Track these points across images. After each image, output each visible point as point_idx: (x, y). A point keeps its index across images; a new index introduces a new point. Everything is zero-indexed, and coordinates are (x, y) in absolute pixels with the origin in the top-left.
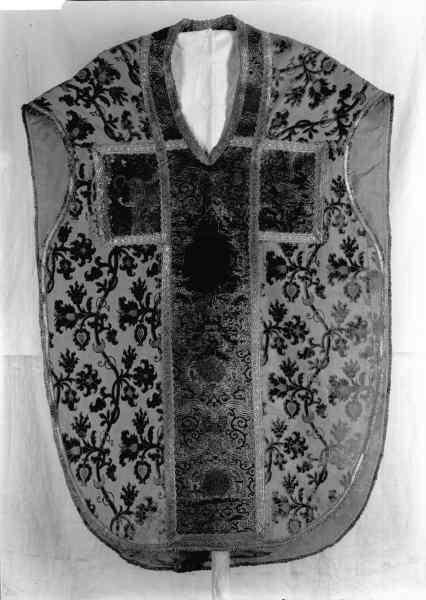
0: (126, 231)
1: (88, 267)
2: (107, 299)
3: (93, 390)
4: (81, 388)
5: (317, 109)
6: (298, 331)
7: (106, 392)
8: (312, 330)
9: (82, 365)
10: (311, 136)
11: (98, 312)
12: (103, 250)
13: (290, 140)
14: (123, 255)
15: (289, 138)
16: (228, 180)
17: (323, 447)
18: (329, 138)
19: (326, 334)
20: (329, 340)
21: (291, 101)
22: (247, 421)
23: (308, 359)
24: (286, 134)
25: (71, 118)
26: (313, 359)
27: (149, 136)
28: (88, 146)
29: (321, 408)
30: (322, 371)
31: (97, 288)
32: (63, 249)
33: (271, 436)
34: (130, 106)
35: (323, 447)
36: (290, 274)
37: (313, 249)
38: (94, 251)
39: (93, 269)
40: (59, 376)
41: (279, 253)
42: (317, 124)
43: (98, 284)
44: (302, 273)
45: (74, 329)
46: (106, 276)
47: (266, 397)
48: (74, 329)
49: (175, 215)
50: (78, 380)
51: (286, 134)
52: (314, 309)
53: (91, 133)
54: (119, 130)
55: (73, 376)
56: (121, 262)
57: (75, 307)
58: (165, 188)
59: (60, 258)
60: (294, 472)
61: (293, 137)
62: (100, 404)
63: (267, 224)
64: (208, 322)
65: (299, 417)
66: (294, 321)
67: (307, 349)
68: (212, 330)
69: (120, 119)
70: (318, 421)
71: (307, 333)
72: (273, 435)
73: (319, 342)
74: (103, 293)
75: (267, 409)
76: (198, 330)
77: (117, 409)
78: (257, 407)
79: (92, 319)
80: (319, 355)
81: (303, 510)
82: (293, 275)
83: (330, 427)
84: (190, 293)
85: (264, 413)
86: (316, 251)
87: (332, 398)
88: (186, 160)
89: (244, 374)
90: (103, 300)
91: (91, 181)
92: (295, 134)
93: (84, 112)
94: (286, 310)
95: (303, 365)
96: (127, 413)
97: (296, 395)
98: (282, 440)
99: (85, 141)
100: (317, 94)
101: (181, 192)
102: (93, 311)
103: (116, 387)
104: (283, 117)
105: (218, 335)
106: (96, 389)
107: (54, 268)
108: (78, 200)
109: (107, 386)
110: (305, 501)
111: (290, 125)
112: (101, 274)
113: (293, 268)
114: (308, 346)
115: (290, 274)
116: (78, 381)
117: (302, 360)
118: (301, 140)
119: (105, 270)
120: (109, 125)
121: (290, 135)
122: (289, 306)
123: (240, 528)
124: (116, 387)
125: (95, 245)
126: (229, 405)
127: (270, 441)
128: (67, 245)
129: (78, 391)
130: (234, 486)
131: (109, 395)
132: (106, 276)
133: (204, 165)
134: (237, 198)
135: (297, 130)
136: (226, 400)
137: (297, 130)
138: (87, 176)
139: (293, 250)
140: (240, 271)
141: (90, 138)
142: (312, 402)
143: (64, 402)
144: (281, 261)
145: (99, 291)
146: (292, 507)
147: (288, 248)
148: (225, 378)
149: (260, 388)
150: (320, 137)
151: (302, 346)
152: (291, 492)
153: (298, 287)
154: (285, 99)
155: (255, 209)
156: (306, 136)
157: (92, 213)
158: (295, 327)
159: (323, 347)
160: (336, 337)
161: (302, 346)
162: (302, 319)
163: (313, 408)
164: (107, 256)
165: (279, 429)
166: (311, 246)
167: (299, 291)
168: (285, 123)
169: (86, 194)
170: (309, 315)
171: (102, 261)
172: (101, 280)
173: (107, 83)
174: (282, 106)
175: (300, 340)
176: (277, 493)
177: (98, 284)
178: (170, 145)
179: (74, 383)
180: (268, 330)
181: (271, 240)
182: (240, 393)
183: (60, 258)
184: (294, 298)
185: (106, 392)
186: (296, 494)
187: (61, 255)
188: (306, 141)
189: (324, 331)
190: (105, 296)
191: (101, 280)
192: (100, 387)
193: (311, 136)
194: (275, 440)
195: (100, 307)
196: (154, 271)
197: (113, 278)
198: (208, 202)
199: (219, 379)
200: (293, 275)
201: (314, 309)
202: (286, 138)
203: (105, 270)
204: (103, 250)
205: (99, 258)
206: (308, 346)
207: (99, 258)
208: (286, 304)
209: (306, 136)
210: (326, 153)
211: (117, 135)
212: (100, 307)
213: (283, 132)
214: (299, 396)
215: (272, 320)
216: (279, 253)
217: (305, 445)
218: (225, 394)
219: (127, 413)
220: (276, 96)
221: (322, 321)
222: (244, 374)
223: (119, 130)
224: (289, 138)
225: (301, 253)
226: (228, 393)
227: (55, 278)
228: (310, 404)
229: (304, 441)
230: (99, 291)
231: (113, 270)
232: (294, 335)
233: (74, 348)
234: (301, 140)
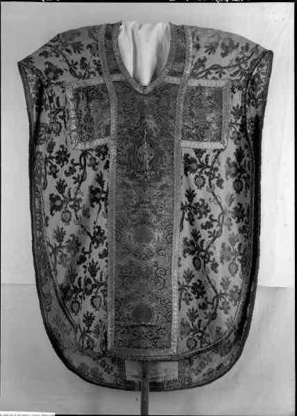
0: (91, 138)
1: (67, 167)
2: (81, 188)
3: (65, 162)
4: (58, 163)
5: (226, 58)
6: (202, 210)
7: (85, 250)
8: (212, 210)
9: (69, 235)
10: (220, 76)
11: (75, 198)
12: (75, 155)
13: (207, 78)
14: (89, 156)
15: (205, 76)
16: (158, 102)
17: (214, 294)
18: (233, 78)
19: (222, 214)
20: (218, 302)
21: (209, 51)
22: (167, 271)
23: (208, 230)
24: (204, 74)
25: (47, 66)
26: (212, 230)
27: (101, 73)
28: (59, 83)
29: (215, 266)
30: (217, 239)
31: (74, 181)
32: (51, 158)
33: (183, 281)
34: (87, 53)
35: (214, 294)
36: (199, 170)
37: (216, 153)
38: (69, 156)
39: (70, 168)
40: (54, 246)
41: (193, 155)
42: (225, 68)
43: (74, 178)
44: (208, 170)
45: (61, 211)
46: (79, 172)
47: (181, 254)
48: (43, 72)
49: (120, 126)
50: (68, 246)
51: (204, 74)
52: (214, 195)
53: (61, 74)
54: (79, 70)
55: (63, 244)
56: (88, 161)
57: (61, 196)
58: (113, 110)
59: (59, 253)
60: (196, 308)
61: (209, 76)
62: (72, 170)
63: (188, 136)
64: (142, 202)
65: (204, 188)
66: (201, 203)
67: (207, 222)
68: (145, 207)
69: (79, 62)
70: (217, 190)
71: (209, 211)
72: (184, 280)
73: (211, 301)
74: (77, 184)
75: (182, 262)
76: (136, 207)
77: (85, 173)
78: (175, 260)
79: (72, 203)
80: (215, 227)
81: (200, 334)
82: (201, 171)
83: (220, 280)
84: (131, 182)
85: (179, 266)
86: (218, 155)
87: (222, 259)
88: (127, 87)
89: (166, 238)
90: (67, 61)
91: (64, 107)
92: (210, 73)
93: (58, 62)
94: (196, 194)
95: (204, 234)
96: (91, 174)
97: (203, 172)
98: (54, 154)
99: (58, 81)
100: (227, 47)
101: (124, 110)
102: (82, 287)
103: (82, 159)
104: (201, 62)
105: (149, 211)
106: (68, 161)
107: (46, 172)
108: (58, 122)
109: (75, 158)
110: (202, 329)
111: (207, 68)
112: (75, 171)
113: (202, 166)
114: (209, 220)
115: (199, 170)
116: (57, 158)
117: (203, 230)
118: (214, 78)
119: (77, 168)
120: (80, 180)
121: (206, 74)
122: (197, 192)
123: (158, 345)
124: (82, 159)
125: (70, 151)
126: (153, 260)
127: (181, 283)
128: (54, 154)
129: (57, 165)
130: (155, 316)
131: (77, 164)
132: (79, 172)
133: (140, 94)
134: (164, 115)
135: (211, 71)
136: (152, 256)
137: (211, 71)
138: (62, 104)
139: (202, 154)
140: (165, 166)
141: (61, 79)
142: (214, 177)
143: (50, 174)
144: (194, 161)
145: (75, 183)
146: (191, 330)
147: (199, 152)
148: (152, 241)
149: (178, 247)
150: (226, 76)
151: (205, 220)
152: (193, 321)
153: (204, 179)
154: (195, 309)
155: (180, 123)
156: (217, 76)
157: (67, 130)
158: (198, 287)
159: (219, 222)
160: (223, 300)
161: (205, 220)
162: (205, 202)
163: (214, 181)
164: (79, 157)
165: (189, 276)
166: (214, 151)
167: (204, 182)
168: (204, 66)
169: (63, 117)
170: (210, 199)
171: (75, 162)
172: (75, 175)
173: (71, 39)
174: (202, 54)
175: (204, 216)
176: (183, 319)
177: (74, 178)
178: (116, 77)
179: (54, 160)
180: (183, 208)
181: (188, 146)
182: (162, 330)
183: (59, 253)
184: (201, 187)
185: (85, 250)
186: (196, 323)
187: (60, 251)
188: (217, 79)
189: (220, 211)
190: (80, 185)
191: (75, 175)
192: (70, 159)
193: (220, 76)
194: (186, 284)
195: (76, 194)
196: (107, 166)
197: (83, 173)
198: (143, 118)
199: (149, 241)
200: (201, 171)
201: (214, 195)
202: (204, 76)
203: (77, 168)
204: (75, 155)
205: (73, 160)
206: (209, 220)
207: (73, 160)
208: (196, 190)
209: (217, 76)
210: (229, 90)
211: (78, 74)
212: (76, 194)
213: (202, 72)
214: (205, 172)
215: (187, 201)
216: (193, 155)
217: (208, 209)
218: (151, 252)
219: (91, 174)
220: (197, 47)
221: (219, 204)
222: (166, 238)
223: (79, 70)
224: (205, 76)
225: (208, 155)
226: (154, 251)
227: (47, 178)
228: (207, 262)
229: (207, 206)
230: (75, 183)
231: (83, 167)
232: (199, 211)
233: (62, 225)
234: (214, 78)
